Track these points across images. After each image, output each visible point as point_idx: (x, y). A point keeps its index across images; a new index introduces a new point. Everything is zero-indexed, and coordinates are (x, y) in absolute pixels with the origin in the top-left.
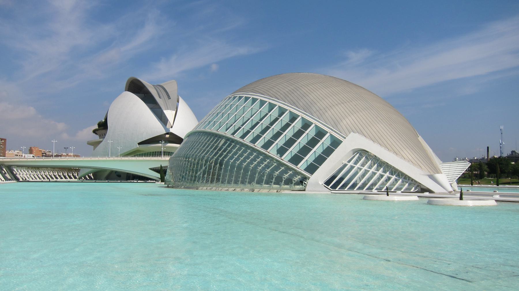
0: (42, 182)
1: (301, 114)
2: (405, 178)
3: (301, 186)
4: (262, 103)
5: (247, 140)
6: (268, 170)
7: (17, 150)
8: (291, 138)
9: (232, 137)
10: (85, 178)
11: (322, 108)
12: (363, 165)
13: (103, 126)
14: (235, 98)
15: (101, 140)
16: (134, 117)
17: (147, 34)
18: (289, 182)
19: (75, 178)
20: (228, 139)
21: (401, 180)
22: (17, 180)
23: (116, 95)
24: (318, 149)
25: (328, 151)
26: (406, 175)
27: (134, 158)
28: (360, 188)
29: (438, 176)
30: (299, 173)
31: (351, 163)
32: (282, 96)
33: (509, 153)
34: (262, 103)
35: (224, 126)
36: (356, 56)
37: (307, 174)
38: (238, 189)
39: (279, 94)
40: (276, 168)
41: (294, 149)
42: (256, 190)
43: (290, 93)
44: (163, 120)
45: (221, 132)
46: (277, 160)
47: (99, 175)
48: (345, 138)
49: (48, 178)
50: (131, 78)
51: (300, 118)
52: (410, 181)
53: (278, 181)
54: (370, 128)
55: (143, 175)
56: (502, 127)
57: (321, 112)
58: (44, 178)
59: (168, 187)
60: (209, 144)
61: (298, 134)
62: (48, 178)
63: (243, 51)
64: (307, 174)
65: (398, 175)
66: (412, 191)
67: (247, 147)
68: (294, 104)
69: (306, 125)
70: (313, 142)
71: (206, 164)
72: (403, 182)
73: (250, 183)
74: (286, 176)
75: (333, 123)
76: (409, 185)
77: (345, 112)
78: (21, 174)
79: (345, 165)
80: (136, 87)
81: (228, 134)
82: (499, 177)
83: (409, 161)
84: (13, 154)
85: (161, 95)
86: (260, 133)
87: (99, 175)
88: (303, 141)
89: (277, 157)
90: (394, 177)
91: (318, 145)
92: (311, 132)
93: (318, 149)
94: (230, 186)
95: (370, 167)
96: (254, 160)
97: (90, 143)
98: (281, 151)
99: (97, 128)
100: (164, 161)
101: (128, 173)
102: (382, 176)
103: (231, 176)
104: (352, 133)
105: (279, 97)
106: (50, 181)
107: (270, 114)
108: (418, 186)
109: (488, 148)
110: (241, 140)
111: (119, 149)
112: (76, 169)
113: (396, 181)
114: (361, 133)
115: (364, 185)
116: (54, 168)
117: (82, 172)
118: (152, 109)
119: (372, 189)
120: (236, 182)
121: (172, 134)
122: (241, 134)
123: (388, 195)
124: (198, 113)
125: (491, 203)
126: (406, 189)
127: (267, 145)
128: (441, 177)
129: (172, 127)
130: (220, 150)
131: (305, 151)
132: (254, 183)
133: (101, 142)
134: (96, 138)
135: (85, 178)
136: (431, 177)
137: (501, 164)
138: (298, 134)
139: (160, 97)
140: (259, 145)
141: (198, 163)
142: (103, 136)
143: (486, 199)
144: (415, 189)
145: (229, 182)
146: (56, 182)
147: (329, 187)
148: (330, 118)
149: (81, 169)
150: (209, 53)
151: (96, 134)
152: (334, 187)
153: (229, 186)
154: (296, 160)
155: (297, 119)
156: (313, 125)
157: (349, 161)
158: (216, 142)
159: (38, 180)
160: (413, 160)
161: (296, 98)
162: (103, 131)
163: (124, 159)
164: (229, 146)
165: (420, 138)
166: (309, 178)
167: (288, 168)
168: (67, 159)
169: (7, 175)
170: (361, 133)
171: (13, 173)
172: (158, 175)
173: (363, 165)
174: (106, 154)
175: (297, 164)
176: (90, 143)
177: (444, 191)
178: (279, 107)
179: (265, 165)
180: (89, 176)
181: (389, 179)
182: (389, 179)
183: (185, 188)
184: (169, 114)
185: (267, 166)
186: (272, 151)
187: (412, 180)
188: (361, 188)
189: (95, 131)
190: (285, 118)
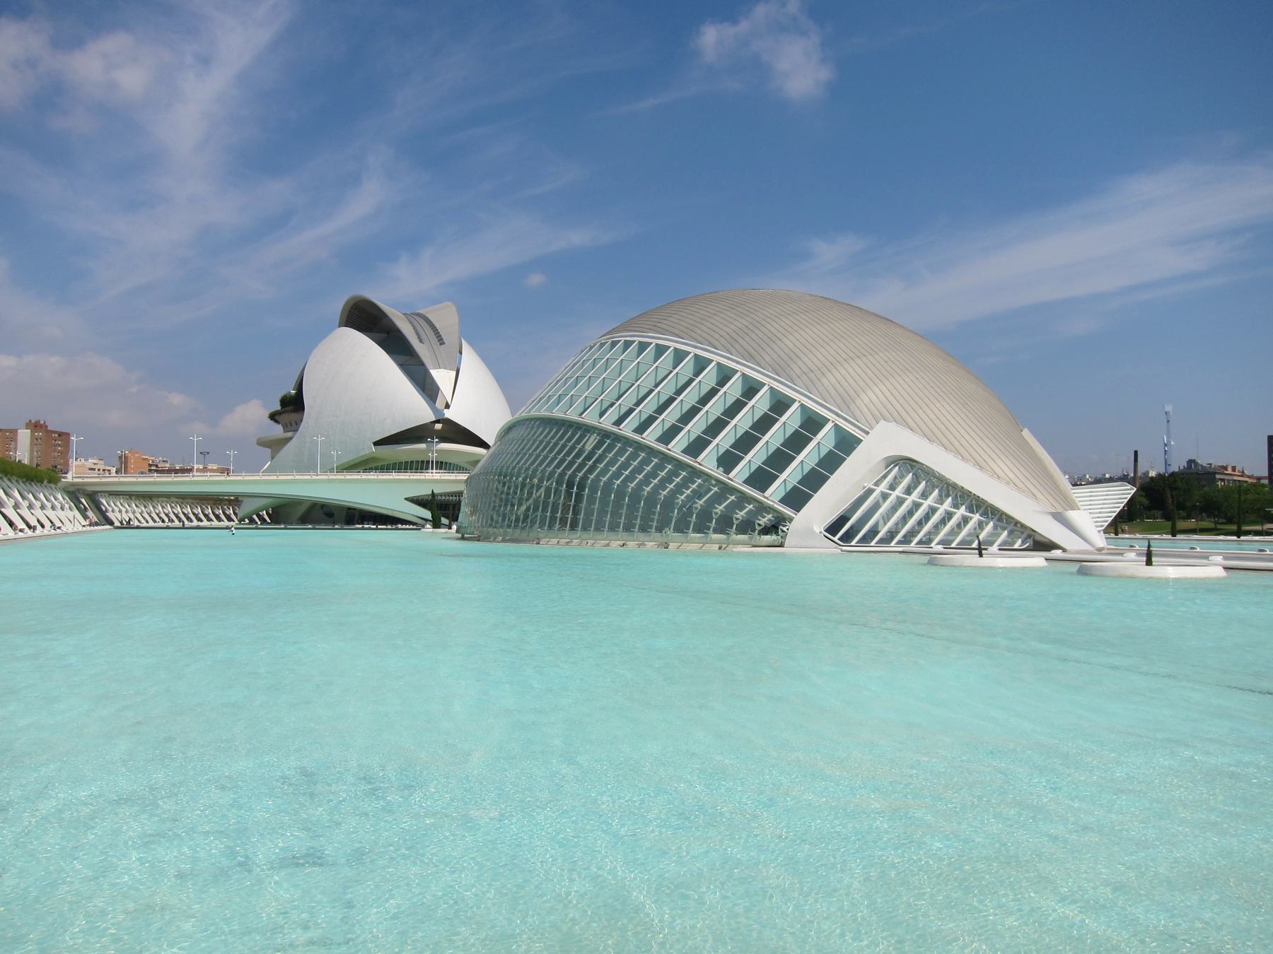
0: (168, 528)
1: (769, 381)
2: (1000, 520)
3: (774, 537)
4: (679, 356)
5: (650, 437)
6: (701, 502)
7: (93, 457)
8: (747, 432)
9: (615, 429)
10: (252, 521)
11: (813, 367)
12: (909, 491)
13: (293, 405)
14: (614, 344)
15: (290, 434)
16: (361, 384)
17: (367, 201)
18: (746, 527)
19: (230, 519)
20: (605, 435)
21: (991, 524)
22: (111, 523)
23: (320, 334)
24: (807, 457)
25: (831, 462)
26: (1003, 513)
27: (365, 476)
28: (882, 541)
29: (1072, 515)
30: (769, 509)
31: (883, 487)
32: (722, 340)
33: (1183, 464)
34: (679, 356)
35: (594, 409)
36: (830, 251)
37: (787, 511)
38: (631, 544)
39: (717, 336)
40: (719, 498)
41: (755, 457)
42: (672, 546)
43: (742, 334)
44: (428, 389)
45: (590, 418)
46: (719, 482)
47: (284, 513)
48: (867, 433)
49: (180, 520)
50: (353, 298)
51: (766, 388)
52: (1011, 527)
53: (724, 525)
54: (920, 412)
55: (390, 513)
56: (1169, 408)
57: (811, 375)
58: (171, 520)
59: (463, 538)
60: (564, 446)
61: (764, 424)
62: (180, 520)
63: (578, 237)
64: (787, 511)
65: (984, 514)
66: (1016, 546)
67: (651, 452)
68: (751, 358)
69: (780, 405)
70: (797, 442)
71: (553, 488)
72: (995, 527)
73: (659, 530)
74: (741, 515)
75: (839, 400)
76: (1011, 533)
77: (863, 375)
78: (118, 510)
79: (869, 492)
80: (365, 318)
81: (607, 423)
82: (334, 523)
83: (1009, 482)
84: (83, 466)
85: (423, 336)
86: (753, 427)
87: (284, 513)
88: (773, 438)
89: (719, 474)
90: (976, 517)
91: (804, 449)
92: (790, 420)
93: (807, 457)
94: (600, 537)
95: (924, 495)
96: (668, 479)
97: (263, 443)
98: (728, 461)
99: (279, 408)
100: (437, 481)
101: (350, 509)
102: (949, 515)
103: (616, 514)
104: (882, 422)
105: (716, 343)
106: (184, 527)
107: (698, 380)
108: (1029, 536)
109: (1136, 453)
110: (637, 437)
111: (337, 457)
112: (230, 501)
113: (981, 525)
114: (901, 422)
115: (891, 535)
116: (183, 498)
117: (247, 507)
118: (402, 366)
119: (910, 542)
120: (628, 528)
121: (448, 423)
122: (636, 424)
123: (981, 555)
124: (505, 376)
125: (1213, 571)
126: (1004, 543)
127: (696, 447)
128: (1078, 517)
129: (447, 406)
130: (589, 458)
131: (779, 460)
132: (669, 532)
133: (291, 438)
134: (277, 430)
135: (251, 520)
136: (1059, 518)
137: (1176, 489)
138: (764, 424)
139: (421, 341)
140: (676, 447)
141: (523, 485)
142: (293, 426)
143: (1197, 565)
144: (1023, 542)
145: (613, 528)
146: (198, 528)
147: (836, 539)
148: (832, 390)
149: (245, 500)
150: (508, 241)
151: (276, 421)
152: (847, 538)
153: (585, 535)
154: (761, 479)
155: (758, 391)
156: (796, 405)
157: (877, 484)
158: (578, 442)
159: (151, 524)
160: (1016, 480)
161: (755, 345)
162: (294, 416)
163: (340, 477)
164: (609, 449)
165: (1026, 433)
166: (791, 520)
167: (744, 499)
168: (208, 477)
169: (90, 514)
170: (901, 422)
171: (100, 509)
172: (427, 514)
173: (909, 491)
174: (310, 467)
175: (763, 489)
176: (263, 443)
177: (1088, 547)
178: (718, 364)
179: (693, 491)
180: (258, 516)
181: (965, 520)
182: (965, 520)
183: (504, 541)
184: (442, 377)
185: (698, 494)
186: (707, 461)
187: (1017, 523)
188: (906, 540)
189: (273, 417)
190: (733, 389)
